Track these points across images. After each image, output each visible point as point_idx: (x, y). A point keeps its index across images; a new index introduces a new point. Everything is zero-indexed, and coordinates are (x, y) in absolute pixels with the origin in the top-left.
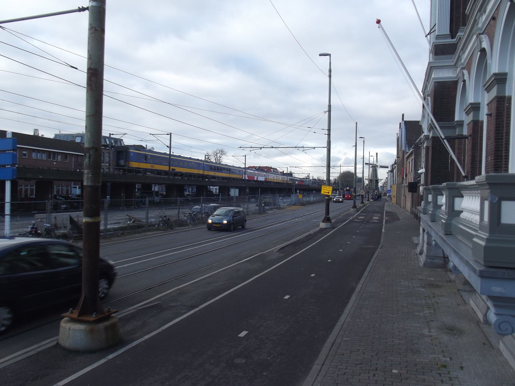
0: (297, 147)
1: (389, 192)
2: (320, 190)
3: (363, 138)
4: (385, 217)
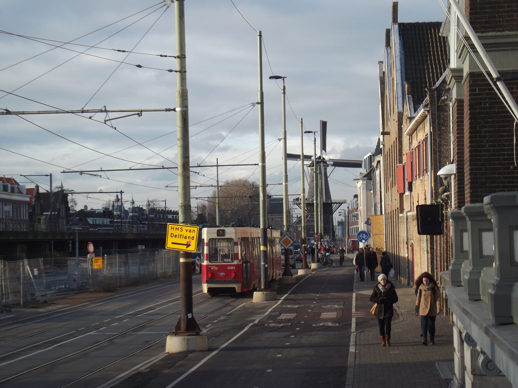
0: (88, 111)
1: (364, 237)
2: (161, 242)
3: (281, 80)
4: (356, 310)
